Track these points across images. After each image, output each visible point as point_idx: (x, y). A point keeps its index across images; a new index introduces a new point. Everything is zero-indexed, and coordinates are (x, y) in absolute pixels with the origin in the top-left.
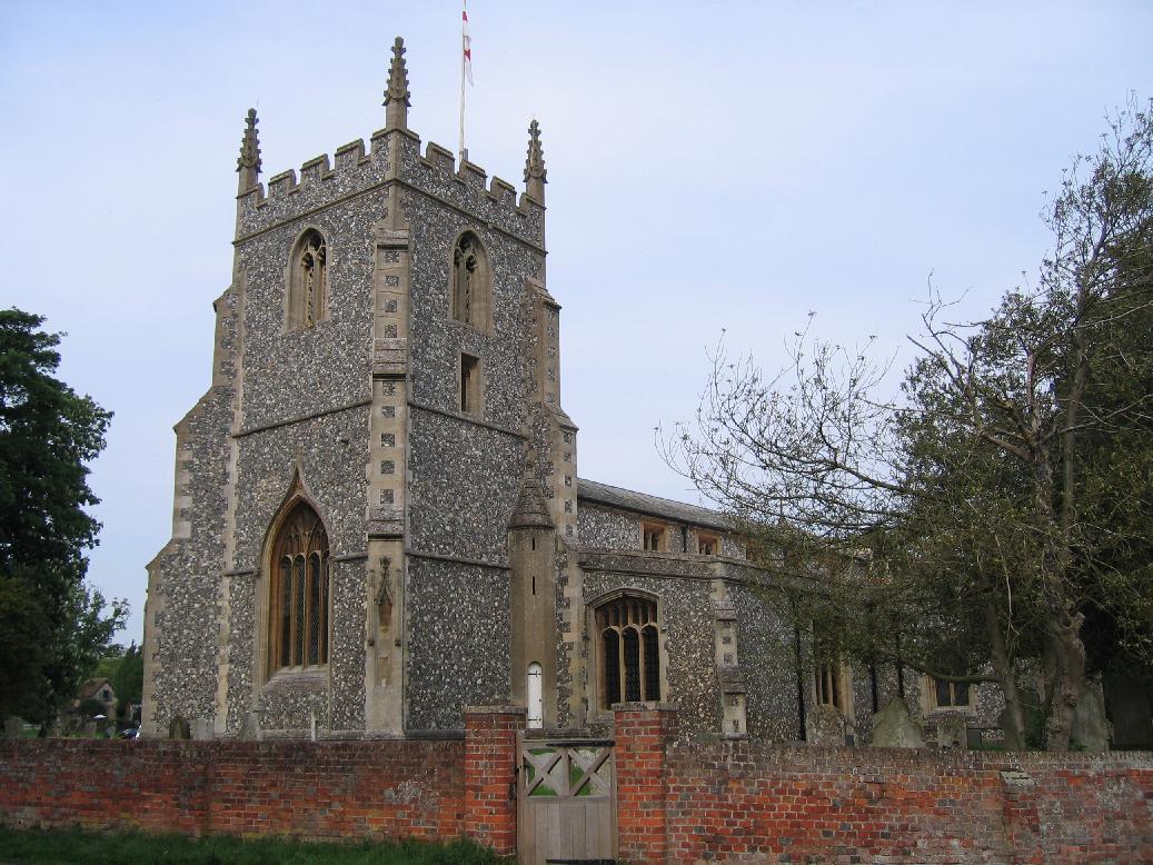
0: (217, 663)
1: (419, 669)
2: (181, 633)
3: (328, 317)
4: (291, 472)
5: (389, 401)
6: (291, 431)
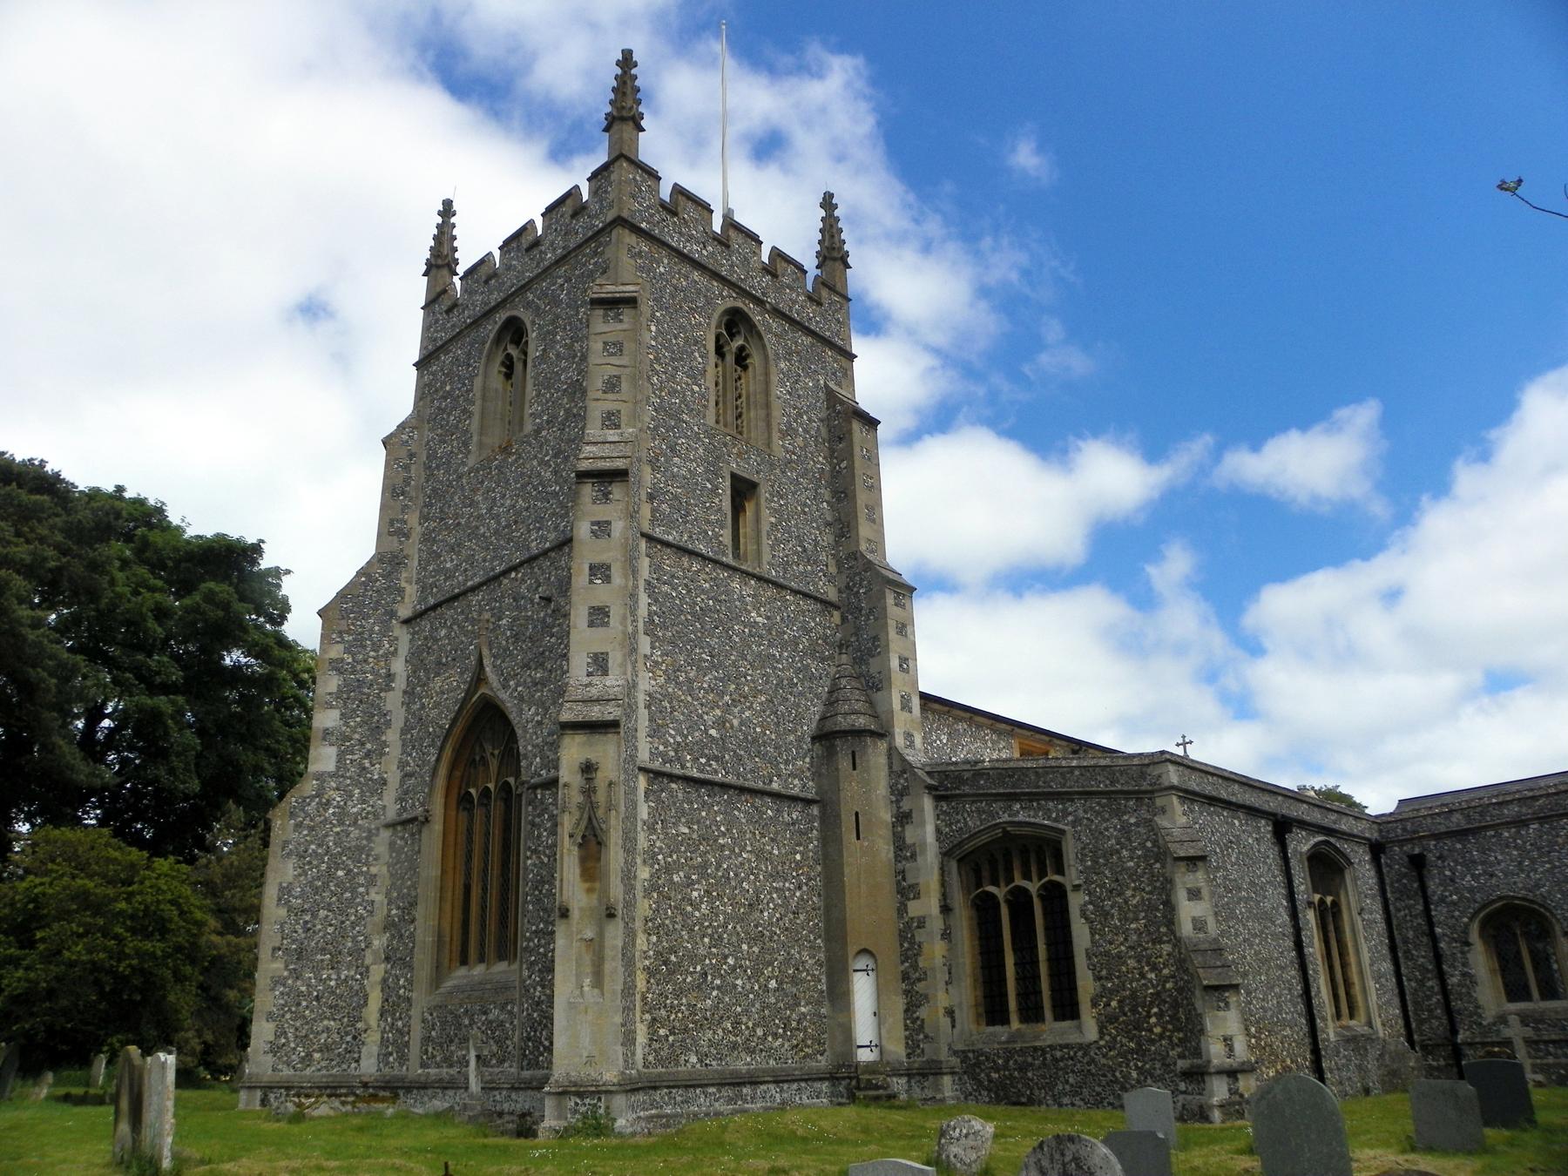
0: (368, 961)
1: (665, 963)
2: (314, 916)
3: (529, 428)
6: (474, 599)
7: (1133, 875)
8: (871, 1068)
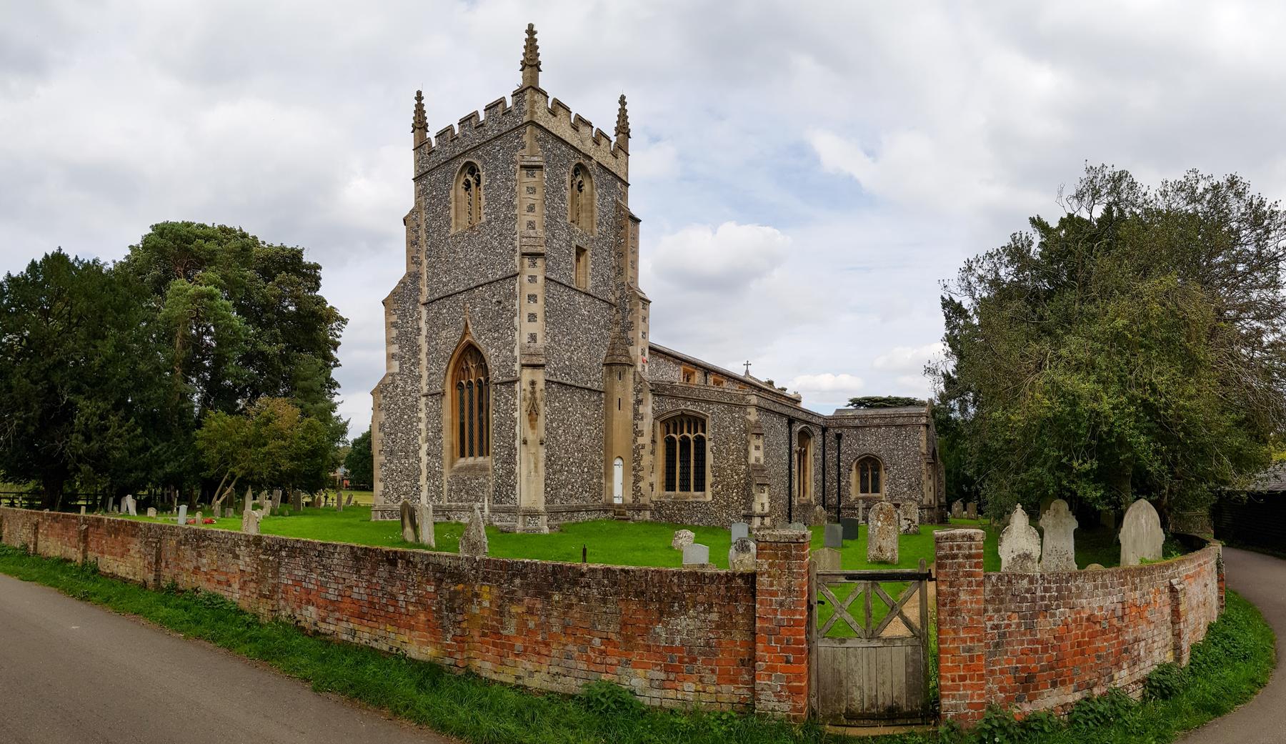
3: (484, 219)
4: (462, 324)
5: (532, 271)
6: (461, 297)
7: (734, 437)
8: (619, 506)
